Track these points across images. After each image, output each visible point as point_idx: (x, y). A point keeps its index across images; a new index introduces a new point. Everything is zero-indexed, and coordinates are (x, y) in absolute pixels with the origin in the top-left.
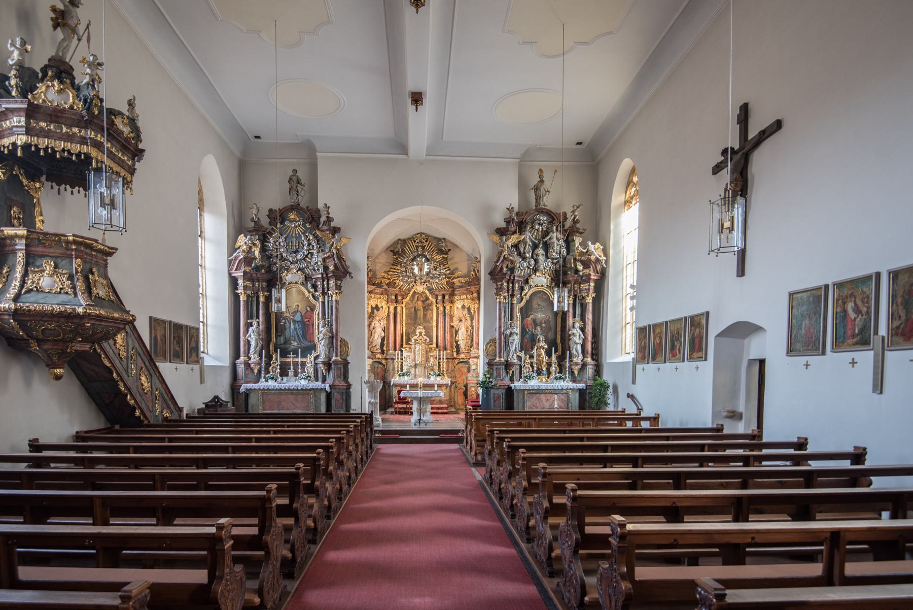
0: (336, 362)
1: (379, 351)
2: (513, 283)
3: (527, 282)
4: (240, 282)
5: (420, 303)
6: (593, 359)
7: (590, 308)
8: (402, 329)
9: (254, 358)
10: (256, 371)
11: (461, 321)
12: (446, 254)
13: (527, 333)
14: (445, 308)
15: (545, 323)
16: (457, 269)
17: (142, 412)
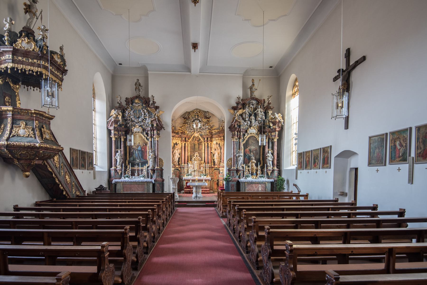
0: (157, 169)
1: (177, 164)
2: (240, 132)
3: (246, 132)
4: (112, 132)
5: (196, 141)
6: (277, 168)
7: (276, 144)
8: (188, 154)
9: (119, 167)
10: (120, 173)
11: (215, 150)
12: (209, 118)
13: (246, 155)
14: (208, 144)
15: (255, 151)
16: (214, 126)
17: (67, 193)
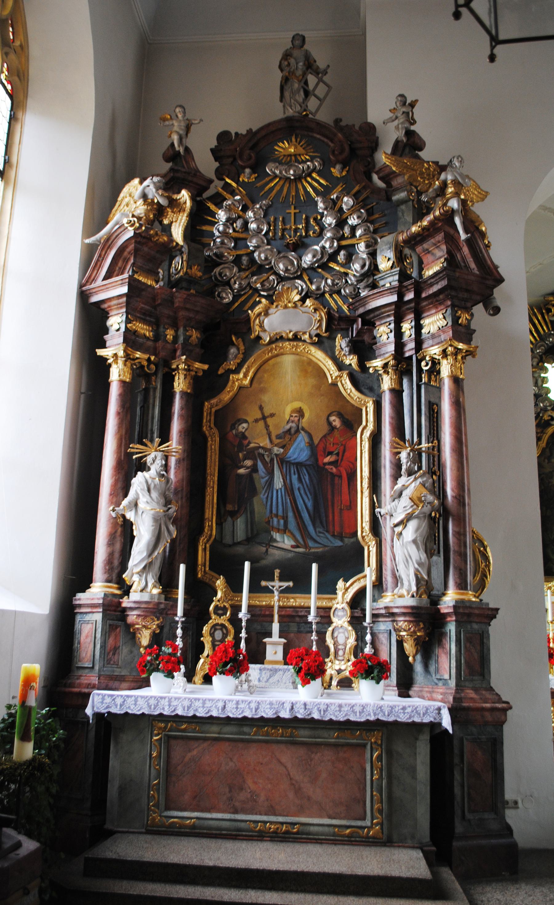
4: (116, 321)
9: (143, 589)
10: (145, 639)
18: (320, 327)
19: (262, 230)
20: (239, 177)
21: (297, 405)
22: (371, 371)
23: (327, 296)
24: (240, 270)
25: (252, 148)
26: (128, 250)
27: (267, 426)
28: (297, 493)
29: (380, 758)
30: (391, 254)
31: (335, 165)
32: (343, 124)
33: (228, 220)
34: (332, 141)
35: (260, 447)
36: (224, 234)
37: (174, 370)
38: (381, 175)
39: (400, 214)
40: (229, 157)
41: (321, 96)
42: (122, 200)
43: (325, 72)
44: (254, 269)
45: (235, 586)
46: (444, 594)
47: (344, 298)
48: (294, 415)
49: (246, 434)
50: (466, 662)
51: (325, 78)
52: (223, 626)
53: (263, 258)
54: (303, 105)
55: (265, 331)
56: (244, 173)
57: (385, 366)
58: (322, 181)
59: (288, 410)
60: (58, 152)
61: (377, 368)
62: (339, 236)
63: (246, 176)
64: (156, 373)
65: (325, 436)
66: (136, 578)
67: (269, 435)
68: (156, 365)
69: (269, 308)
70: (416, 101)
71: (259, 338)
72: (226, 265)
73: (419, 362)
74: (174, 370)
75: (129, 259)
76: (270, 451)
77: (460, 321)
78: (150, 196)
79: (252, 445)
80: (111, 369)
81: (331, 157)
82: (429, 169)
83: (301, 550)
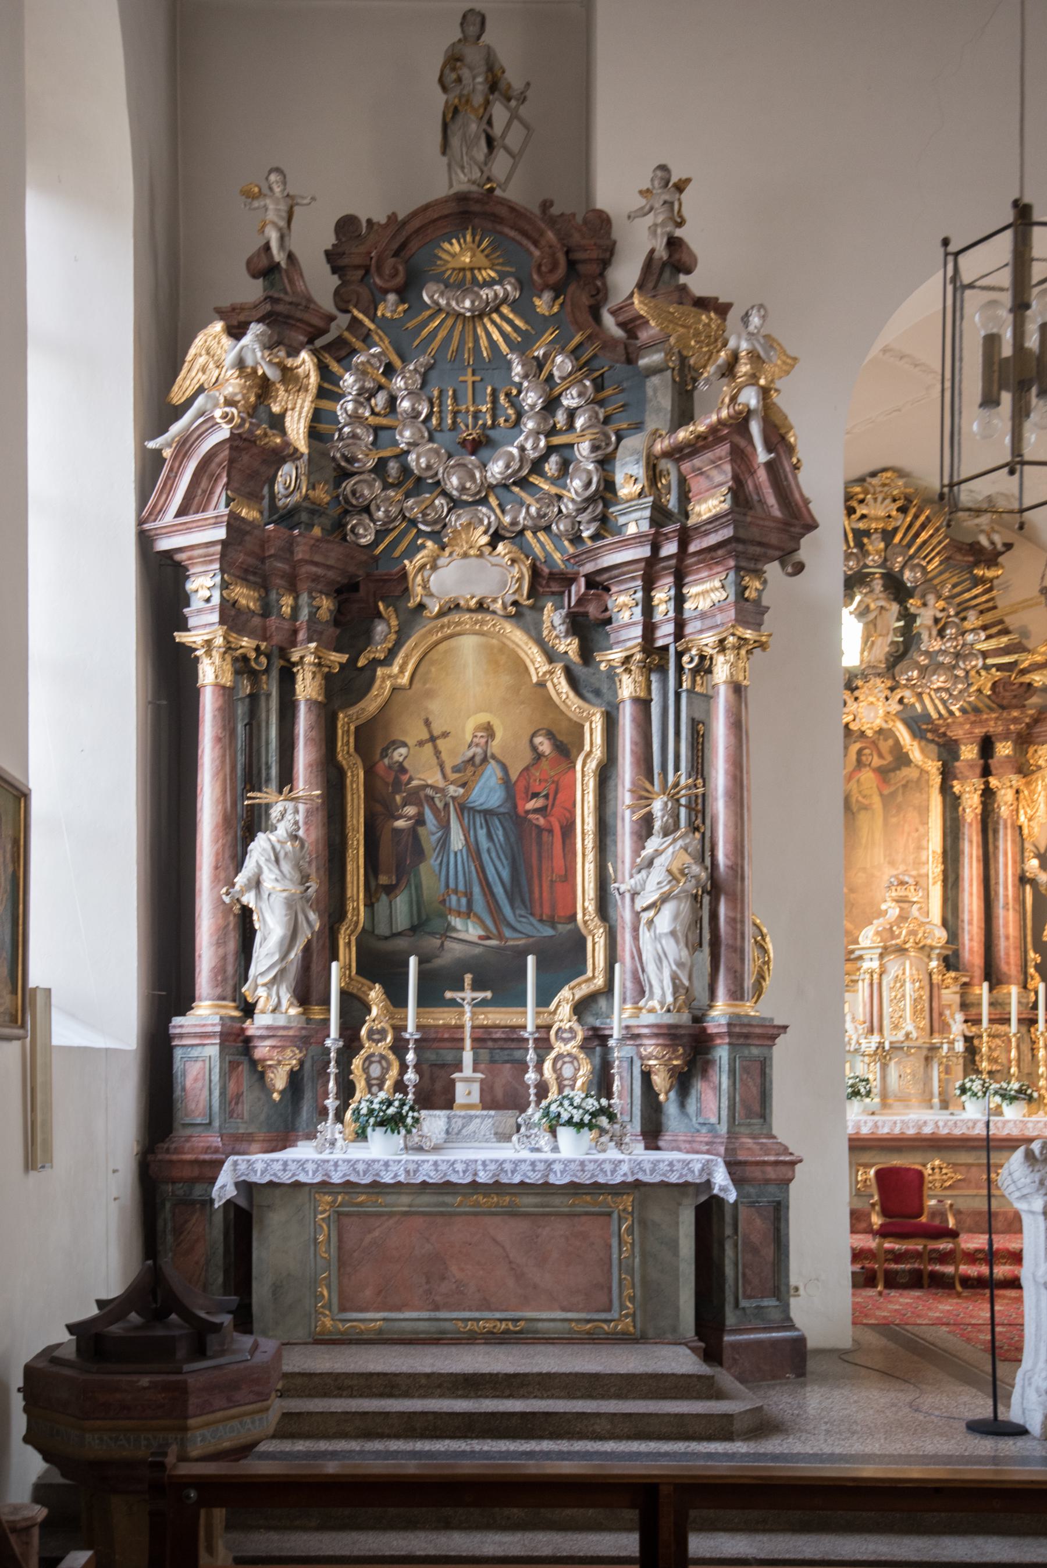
4: (204, 585)
9: (275, 1009)
10: (279, 1080)
14: (988, 794)
18: (519, 589)
19: (420, 414)
20: (376, 309)
21: (483, 718)
22: (603, 667)
23: (529, 534)
24: (386, 486)
25: (396, 254)
26: (217, 460)
27: (437, 753)
28: (485, 857)
29: (630, 1231)
30: (639, 470)
31: (542, 291)
32: (555, 211)
33: (361, 391)
34: (536, 243)
35: (428, 786)
36: (355, 418)
37: (294, 664)
38: (621, 319)
39: (650, 392)
40: (357, 267)
41: (515, 149)
42: (193, 360)
43: (523, 99)
44: (409, 484)
45: (396, 998)
46: (711, 1007)
47: (556, 538)
48: (480, 734)
49: (406, 764)
50: (741, 1100)
51: (523, 110)
52: (383, 1057)
53: (423, 465)
54: (485, 169)
55: (431, 595)
56: (385, 300)
57: (627, 659)
58: (518, 322)
59: (470, 725)
60: (81, 272)
61: (613, 664)
62: (548, 428)
63: (389, 307)
64: (267, 671)
65: (527, 769)
66: (262, 992)
67: (442, 766)
68: (268, 657)
69: (438, 556)
70: (688, 181)
71: (421, 606)
72: (362, 477)
73: (679, 655)
74: (294, 664)
75: (219, 476)
76: (442, 791)
77: (747, 594)
78: (249, 362)
79: (415, 783)
80: (200, 667)
81: (535, 277)
82: (708, 325)
83: (493, 942)
